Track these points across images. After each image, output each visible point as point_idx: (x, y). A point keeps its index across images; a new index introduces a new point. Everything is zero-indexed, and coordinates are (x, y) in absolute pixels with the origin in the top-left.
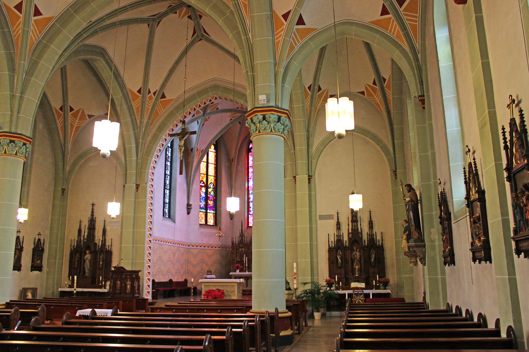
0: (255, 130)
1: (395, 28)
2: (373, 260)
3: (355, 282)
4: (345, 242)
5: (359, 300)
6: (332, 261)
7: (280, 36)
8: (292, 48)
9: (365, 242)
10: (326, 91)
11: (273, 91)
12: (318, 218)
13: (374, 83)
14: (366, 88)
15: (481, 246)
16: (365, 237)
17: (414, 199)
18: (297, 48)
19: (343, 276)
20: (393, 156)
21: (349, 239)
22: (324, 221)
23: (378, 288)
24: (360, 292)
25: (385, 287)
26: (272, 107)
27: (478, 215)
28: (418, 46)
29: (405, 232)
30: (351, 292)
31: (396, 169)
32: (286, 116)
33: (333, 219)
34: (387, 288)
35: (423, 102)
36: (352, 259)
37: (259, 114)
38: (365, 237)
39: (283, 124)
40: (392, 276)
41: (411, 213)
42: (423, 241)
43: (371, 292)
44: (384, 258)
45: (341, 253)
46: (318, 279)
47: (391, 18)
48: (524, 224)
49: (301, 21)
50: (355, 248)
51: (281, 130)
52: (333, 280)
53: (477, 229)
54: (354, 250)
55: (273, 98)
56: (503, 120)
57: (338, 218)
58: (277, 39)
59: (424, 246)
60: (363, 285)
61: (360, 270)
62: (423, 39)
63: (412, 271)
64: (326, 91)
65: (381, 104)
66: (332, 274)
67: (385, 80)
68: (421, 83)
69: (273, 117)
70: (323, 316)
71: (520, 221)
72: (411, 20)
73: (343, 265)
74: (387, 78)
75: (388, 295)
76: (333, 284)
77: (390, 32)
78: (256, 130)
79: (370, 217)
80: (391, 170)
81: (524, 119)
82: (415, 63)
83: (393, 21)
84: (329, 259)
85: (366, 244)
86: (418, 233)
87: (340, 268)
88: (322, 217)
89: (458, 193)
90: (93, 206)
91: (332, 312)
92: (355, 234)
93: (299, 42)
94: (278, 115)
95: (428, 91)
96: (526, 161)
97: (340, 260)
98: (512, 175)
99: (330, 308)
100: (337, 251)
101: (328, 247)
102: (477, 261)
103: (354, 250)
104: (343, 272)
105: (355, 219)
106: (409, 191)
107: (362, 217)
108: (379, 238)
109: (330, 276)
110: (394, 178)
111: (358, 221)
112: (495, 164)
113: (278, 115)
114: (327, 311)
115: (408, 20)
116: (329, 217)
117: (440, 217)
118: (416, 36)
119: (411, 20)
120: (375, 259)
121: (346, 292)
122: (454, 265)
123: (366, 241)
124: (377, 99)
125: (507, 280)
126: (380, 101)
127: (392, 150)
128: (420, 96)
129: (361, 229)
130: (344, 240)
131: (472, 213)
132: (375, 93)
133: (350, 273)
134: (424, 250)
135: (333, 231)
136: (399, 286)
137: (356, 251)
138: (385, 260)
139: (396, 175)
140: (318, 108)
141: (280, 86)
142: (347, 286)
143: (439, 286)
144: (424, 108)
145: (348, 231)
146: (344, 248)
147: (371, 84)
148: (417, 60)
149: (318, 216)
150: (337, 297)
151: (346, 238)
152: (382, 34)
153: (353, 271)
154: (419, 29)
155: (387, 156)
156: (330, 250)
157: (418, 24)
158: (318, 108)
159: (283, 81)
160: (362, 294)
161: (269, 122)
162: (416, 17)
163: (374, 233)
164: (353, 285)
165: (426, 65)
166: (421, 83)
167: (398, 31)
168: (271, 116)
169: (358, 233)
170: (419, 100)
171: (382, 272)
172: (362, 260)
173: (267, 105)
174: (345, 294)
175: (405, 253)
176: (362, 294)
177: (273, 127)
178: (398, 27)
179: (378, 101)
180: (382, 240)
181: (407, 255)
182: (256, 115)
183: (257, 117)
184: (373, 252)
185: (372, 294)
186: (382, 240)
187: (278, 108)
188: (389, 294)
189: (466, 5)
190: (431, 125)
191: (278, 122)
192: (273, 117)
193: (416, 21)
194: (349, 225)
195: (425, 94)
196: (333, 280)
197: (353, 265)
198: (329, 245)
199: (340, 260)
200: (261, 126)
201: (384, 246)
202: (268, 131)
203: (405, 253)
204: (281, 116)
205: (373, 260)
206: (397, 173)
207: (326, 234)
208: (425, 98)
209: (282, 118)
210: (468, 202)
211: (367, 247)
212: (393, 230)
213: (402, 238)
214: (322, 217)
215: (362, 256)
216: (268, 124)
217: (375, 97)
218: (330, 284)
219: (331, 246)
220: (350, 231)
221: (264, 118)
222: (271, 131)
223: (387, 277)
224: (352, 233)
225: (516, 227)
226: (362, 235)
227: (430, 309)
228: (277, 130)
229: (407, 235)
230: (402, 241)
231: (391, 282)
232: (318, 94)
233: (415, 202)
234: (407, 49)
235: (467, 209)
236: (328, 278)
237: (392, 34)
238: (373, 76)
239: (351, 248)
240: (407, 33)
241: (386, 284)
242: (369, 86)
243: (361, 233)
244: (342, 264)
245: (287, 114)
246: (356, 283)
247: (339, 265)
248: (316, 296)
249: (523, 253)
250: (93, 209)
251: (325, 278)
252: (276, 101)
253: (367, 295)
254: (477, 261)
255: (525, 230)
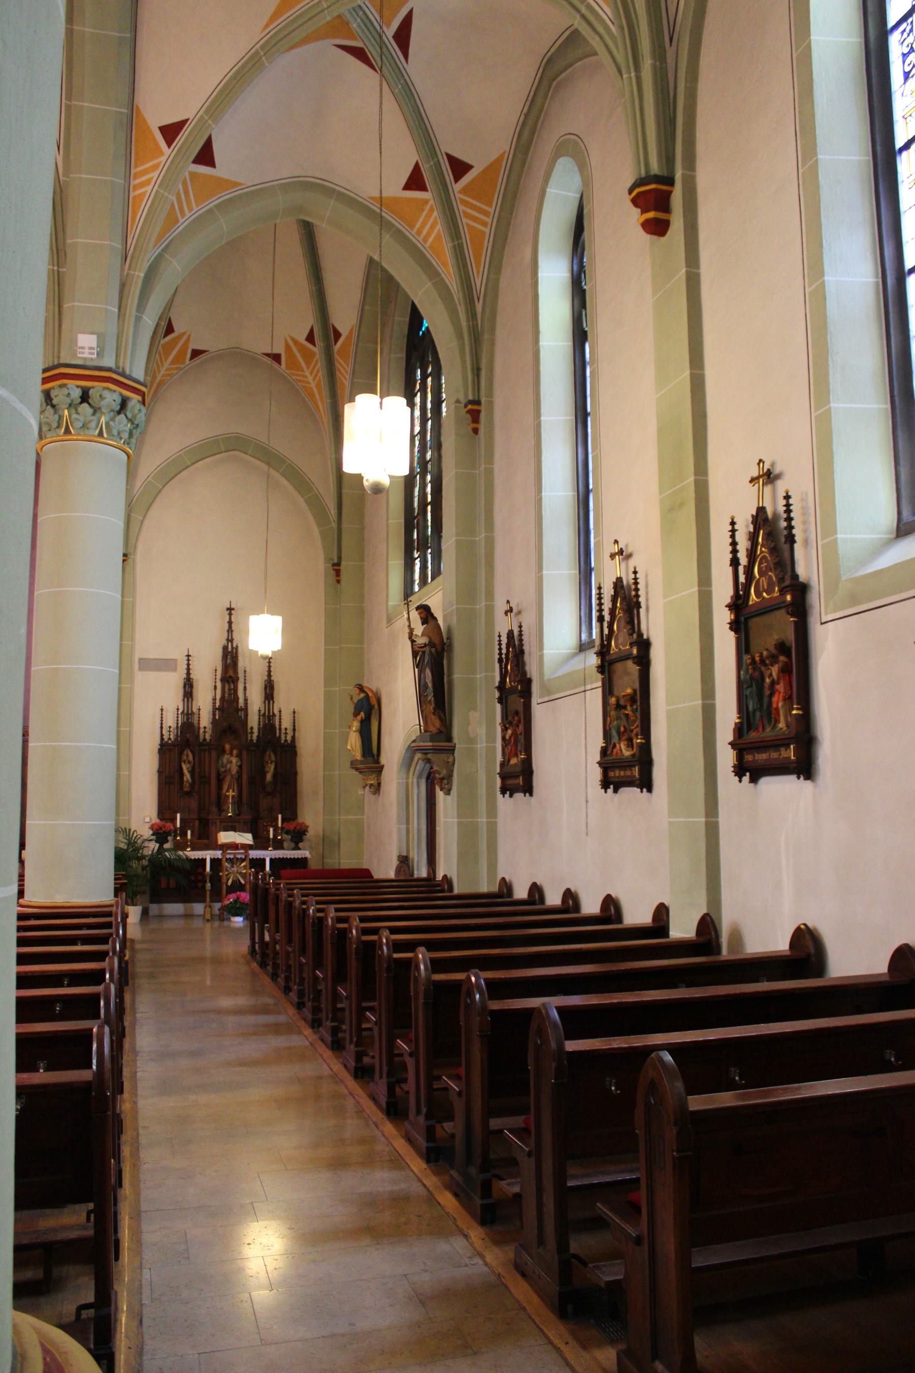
0: (55, 425)
1: (433, 227)
2: (269, 777)
3: (226, 830)
4: (202, 730)
5: (234, 873)
6: (168, 778)
7: (148, 182)
8: (172, 220)
9: (252, 733)
10: (185, 337)
11: (113, 329)
12: (136, 667)
13: (310, 338)
14: (288, 347)
15: (633, 755)
16: (253, 721)
17: (437, 641)
18: (183, 223)
19: (195, 816)
20: (334, 525)
21: (214, 722)
22: (152, 676)
23: (278, 845)
24: (240, 854)
25: (297, 843)
26: (109, 370)
27: (629, 691)
28: (479, 282)
29: (356, 714)
30: (218, 854)
31: (340, 558)
32: (140, 398)
33: (175, 670)
34: (300, 845)
35: (475, 416)
36: (218, 774)
37: (71, 383)
38: (253, 721)
39: (131, 421)
40: (311, 814)
41: (428, 673)
42: (449, 739)
43: (268, 855)
44: (296, 774)
45: (273, 758)
46: (129, 820)
47: (426, 202)
48: (762, 717)
49: (206, 156)
50: (227, 747)
51: (125, 435)
52: (169, 826)
53: (624, 722)
54: (224, 751)
55: (111, 345)
56: (734, 502)
57: (188, 669)
58: (136, 188)
59: (452, 750)
60: (246, 838)
61: (238, 802)
62: (496, 266)
63: (361, 808)
64: (185, 337)
65: (320, 393)
66: (165, 809)
67: (337, 335)
68: (477, 371)
69: (110, 397)
70: (145, 913)
71: (754, 712)
72: (475, 219)
73: (196, 788)
74: (344, 330)
75: (303, 862)
76: (169, 834)
77: (419, 233)
78: (59, 427)
79: (269, 672)
80: (327, 559)
81: (792, 515)
82: (468, 321)
83: (432, 210)
84: (160, 772)
85: (208, 737)
86: (440, 718)
87: (188, 794)
88: (147, 664)
89: (560, 635)
90: (230, 614)
91: (165, 905)
92: (229, 709)
93: (190, 210)
94: (121, 395)
95: (490, 394)
96: (789, 598)
97: (187, 776)
98: (742, 619)
99: (158, 895)
100: (181, 753)
101: (158, 741)
102: (612, 786)
103: (224, 751)
104: (194, 803)
105: (231, 673)
106: (424, 621)
107: (248, 670)
108: (286, 723)
109: (161, 813)
110: (332, 578)
111: (238, 679)
112: (699, 591)
113: (121, 395)
114: (152, 902)
115: (467, 215)
116: (166, 665)
117: (501, 687)
118: (478, 257)
119: (475, 219)
120: (275, 776)
121: (208, 855)
122: (531, 795)
123: (256, 730)
124: (310, 379)
125: (703, 827)
126: (318, 386)
127: (333, 511)
128: (471, 402)
129: (246, 700)
130: (202, 726)
131: (608, 689)
132: (308, 363)
133: (214, 809)
134: (451, 760)
135: (173, 701)
136: (329, 842)
137: (231, 754)
138: (299, 778)
139: (338, 573)
140: (159, 378)
141: (133, 319)
142: (206, 839)
143: (480, 840)
144: (476, 431)
145: (214, 703)
146: (201, 744)
147: (302, 338)
148: (472, 314)
149: (136, 660)
150: (188, 866)
151: (205, 721)
152: (399, 235)
153: (220, 803)
154: (488, 243)
155: (319, 525)
156: (165, 749)
157: (487, 230)
158: (159, 378)
159: (141, 307)
160: (243, 860)
161: (96, 410)
162: (486, 214)
163: (276, 712)
164: (225, 837)
165: (493, 329)
166: (477, 371)
167: (438, 238)
168: (106, 394)
169: (238, 710)
170: (468, 412)
171: (290, 808)
172: (245, 776)
173: (95, 364)
174: (204, 860)
175: (354, 765)
176: (243, 860)
177: (107, 424)
178: (439, 227)
179: (313, 385)
180: (294, 730)
181: (357, 769)
182: (61, 386)
183: (65, 391)
184: (270, 756)
185: (271, 860)
186: (294, 730)
187: (123, 374)
188: (305, 860)
189: (663, 239)
190: (489, 473)
191: (119, 413)
192: (110, 397)
193: (484, 224)
194: (215, 687)
195: (483, 400)
196: (169, 826)
197: (220, 788)
198: (162, 735)
199: (187, 776)
200: (74, 416)
201: (297, 744)
202: (91, 432)
203: (354, 765)
204: (89, 388)
205: (269, 777)
206: (342, 568)
207: (156, 705)
208: (483, 408)
209: (130, 405)
210: (602, 661)
211: (257, 746)
212: (320, 706)
213: (350, 727)
214: (147, 664)
215: (245, 769)
216: (94, 414)
217: (307, 373)
218: (160, 835)
219: (166, 738)
220: (218, 704)
221: (85, 397)
222: (101, 434)
223: (300, 820)
224: (221, 709)
225: (741, 723)
226: (246, 715)
227: (456, 891)
228: (115, 432)
229: (362, 722)
230: (348, 733)
231: (311, 833)
232: (163, 341)
233: (439, 648)
234: (453, 283)
235: (600, 676)
236: (155, 820)
237: (420, 239)
238: (307, 320)
239: (216, 746)
240: (461, 246)
241: (298, 836)
242: (295, 342)
243: (246, 709)
244: (192, 785)
245: (142, 394)
246: (232, 833)
247: (187, 788)
248: (134, 864)
249: (748, 774)
250: (230, 623)
251: (147, 820)
252: (117, 356)
253: (258, 864)
254: (612, 786)
255: (764, 729)
